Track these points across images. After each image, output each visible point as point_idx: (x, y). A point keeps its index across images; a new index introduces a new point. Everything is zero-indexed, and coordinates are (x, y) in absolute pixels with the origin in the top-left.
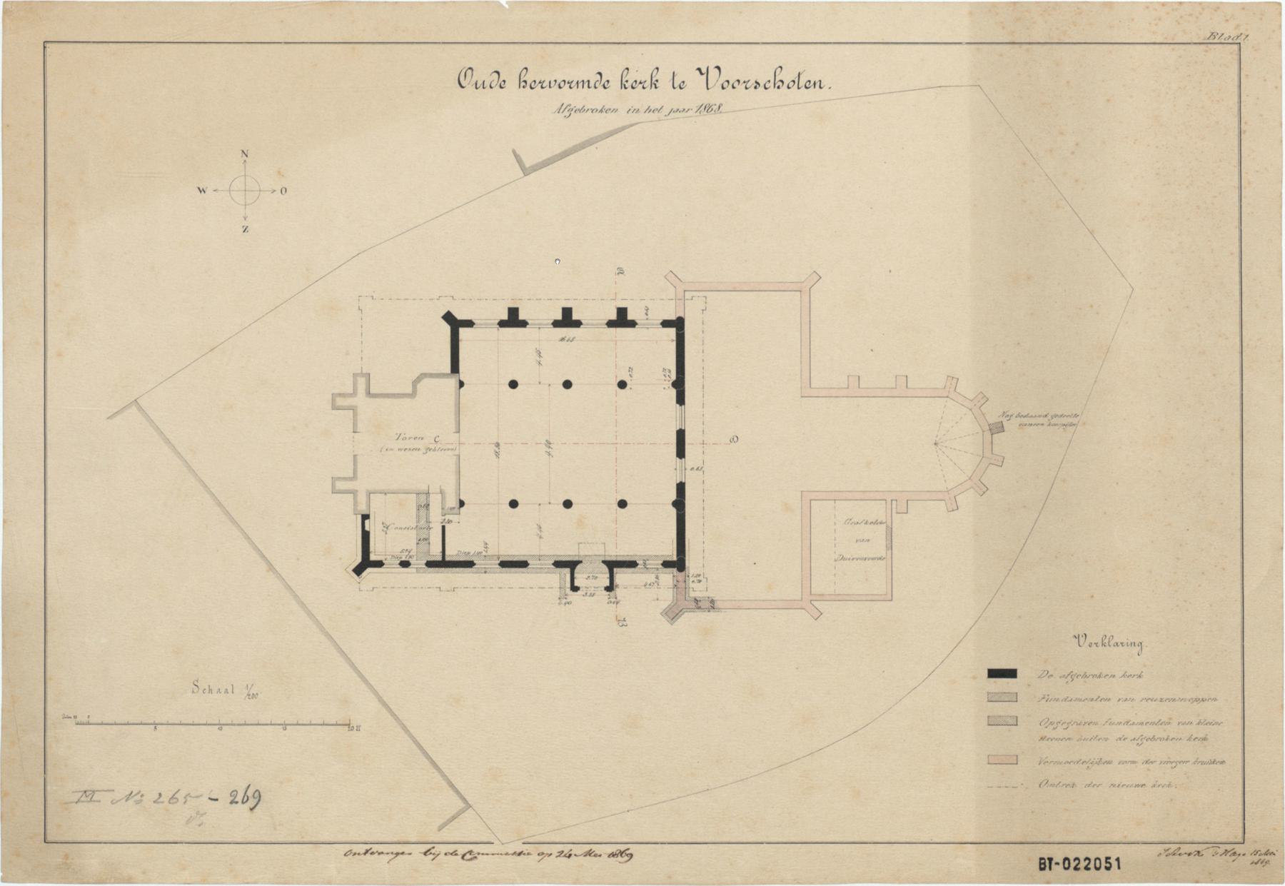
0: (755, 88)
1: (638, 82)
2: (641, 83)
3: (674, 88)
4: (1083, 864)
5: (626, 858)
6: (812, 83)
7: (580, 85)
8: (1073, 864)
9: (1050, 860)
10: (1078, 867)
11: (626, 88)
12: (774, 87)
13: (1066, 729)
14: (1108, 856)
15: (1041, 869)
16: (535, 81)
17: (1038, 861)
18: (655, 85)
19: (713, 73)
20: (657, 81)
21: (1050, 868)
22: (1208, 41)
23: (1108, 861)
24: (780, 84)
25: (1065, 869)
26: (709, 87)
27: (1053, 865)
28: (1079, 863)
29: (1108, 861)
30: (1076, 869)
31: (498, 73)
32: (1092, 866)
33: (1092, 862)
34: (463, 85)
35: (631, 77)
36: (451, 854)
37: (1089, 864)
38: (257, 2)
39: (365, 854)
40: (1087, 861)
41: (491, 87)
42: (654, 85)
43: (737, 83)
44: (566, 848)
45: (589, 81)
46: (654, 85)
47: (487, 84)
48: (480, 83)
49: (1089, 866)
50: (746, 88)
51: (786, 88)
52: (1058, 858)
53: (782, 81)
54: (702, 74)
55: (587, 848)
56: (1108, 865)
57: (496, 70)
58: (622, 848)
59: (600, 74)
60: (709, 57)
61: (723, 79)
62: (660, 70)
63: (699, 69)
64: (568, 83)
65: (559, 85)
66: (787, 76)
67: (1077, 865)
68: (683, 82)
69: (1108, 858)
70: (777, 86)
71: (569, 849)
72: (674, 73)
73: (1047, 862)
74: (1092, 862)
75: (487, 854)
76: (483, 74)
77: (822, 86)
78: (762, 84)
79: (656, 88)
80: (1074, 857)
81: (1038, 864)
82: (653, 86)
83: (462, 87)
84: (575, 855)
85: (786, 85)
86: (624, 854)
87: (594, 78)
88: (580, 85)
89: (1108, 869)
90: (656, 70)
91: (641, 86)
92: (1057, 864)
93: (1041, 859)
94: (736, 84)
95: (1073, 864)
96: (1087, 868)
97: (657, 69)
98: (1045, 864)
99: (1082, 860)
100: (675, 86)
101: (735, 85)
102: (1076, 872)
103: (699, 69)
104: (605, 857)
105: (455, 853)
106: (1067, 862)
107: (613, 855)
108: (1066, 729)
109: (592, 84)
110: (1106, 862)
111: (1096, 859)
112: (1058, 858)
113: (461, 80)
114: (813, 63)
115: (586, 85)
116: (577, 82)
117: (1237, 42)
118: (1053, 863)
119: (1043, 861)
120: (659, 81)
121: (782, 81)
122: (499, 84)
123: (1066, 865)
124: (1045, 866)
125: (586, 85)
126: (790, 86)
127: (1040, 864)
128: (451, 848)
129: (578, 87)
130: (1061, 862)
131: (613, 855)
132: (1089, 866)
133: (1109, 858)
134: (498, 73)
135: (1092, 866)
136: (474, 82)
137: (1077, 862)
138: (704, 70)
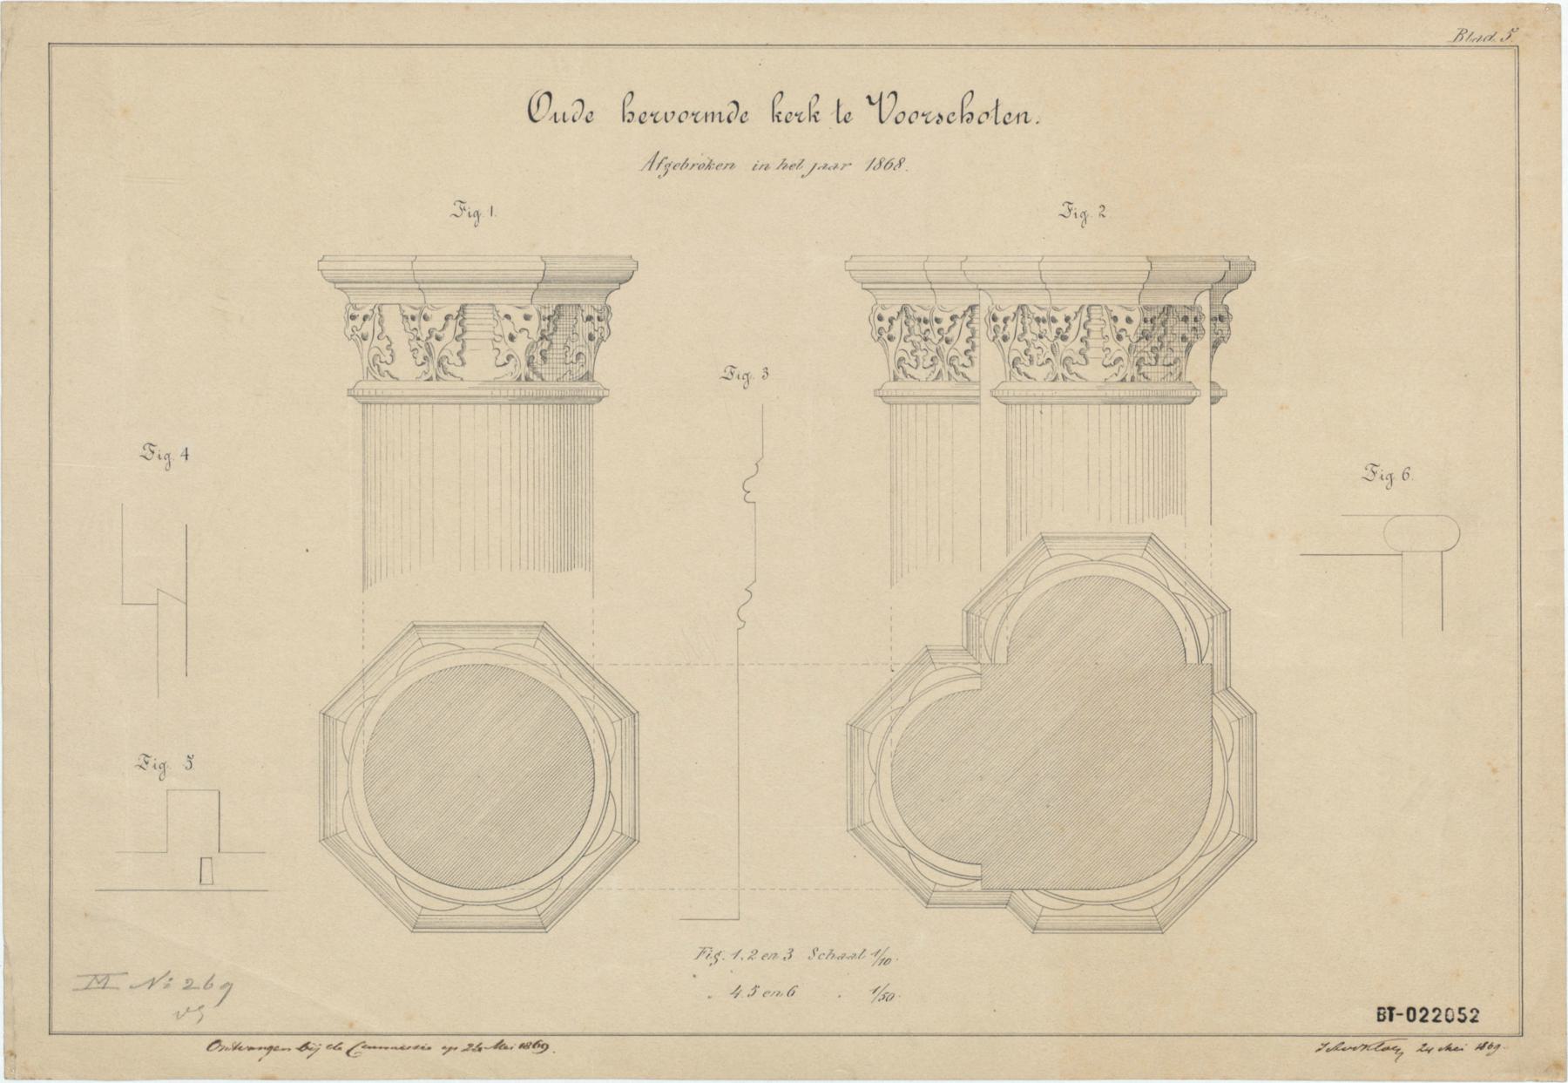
0: (937, 122)
2: (923, 115)
3: (838, 122)
4: (1431, 1016)
5: (540, 1049)
6: (1014, 116)
7: (709, 118)
8: (1419, 1015)
9: (1391, 1009)
10: (1426, 1019)
11: (779, 121)
12: (624, 120)
16: (645, 113)
17: (1377, 1011)
18: (815, 117)
19: (888, 103)
21: (1391, 1019)
24: (970, 116)
25: (1410, 1021)
26: (883, 120)
27: (1395, 1017)
31: (582, 101)
32: (1442, 1018)
34: (535, 118)
36: (334, 1048)
38: (895, 5)
39: (410, 1047)
40: (1424, 1012)
41: (574, 121)
42: (814, 117)
43: (985, 116)
44: (476, 1041)
45: (720, 113)
46: (814, 117)
48: (559, 117)
50: (927, 122)
51: (677, 121)
53: (632, 113)
54: (871, 103)
56: (1462, 1017)
57: (580, 98)
59: (736, 103)
61: (899, 109)
62: (784, 95)
63: (869, 97)
64: (796, 115)
65: (741, 118)
66: (976, 107)
68: (850, 113)
70: (626, 119)
73: (1388, 1012)
74: (1443, 1012)
75: (386, 1048)
76: (562, 104)
77: (1028, 120)
79: (816, 121)
83: (535, 121)
84: (486, 1048)
85: (637, 117)
88: (709, 118)
90: (780, 95)
93: (1379, 1008)
95: (1419, 1015)
97: (782, 93)
100: (840, 120)
101: (982, 120)
103: (869, 97)
105: (337, 1047)
106: (1411, 1012)
107: (522, 1046)
109: (724, 117)
110: (1460, 1013)
111: (1447, 1010)
115: (717, 119)
116: (1018, 116)
118: (1394, 1012)
119: (1382, 1011)
120: (820, 114)
121: (632, 113)
123: (1411, 1017)
124: (1385, 1017)
125: (717, 119)
126: (899, 120)
127: (1379, 1014)
128: (335, 1041)
129: (1018, 122)
130: (1405, 1012)
131: (522, 1046)
134: (582, 101)
135: (1442, 1018)
136: (553, 114)
137: (1424, 1012)
138: (875, 99)
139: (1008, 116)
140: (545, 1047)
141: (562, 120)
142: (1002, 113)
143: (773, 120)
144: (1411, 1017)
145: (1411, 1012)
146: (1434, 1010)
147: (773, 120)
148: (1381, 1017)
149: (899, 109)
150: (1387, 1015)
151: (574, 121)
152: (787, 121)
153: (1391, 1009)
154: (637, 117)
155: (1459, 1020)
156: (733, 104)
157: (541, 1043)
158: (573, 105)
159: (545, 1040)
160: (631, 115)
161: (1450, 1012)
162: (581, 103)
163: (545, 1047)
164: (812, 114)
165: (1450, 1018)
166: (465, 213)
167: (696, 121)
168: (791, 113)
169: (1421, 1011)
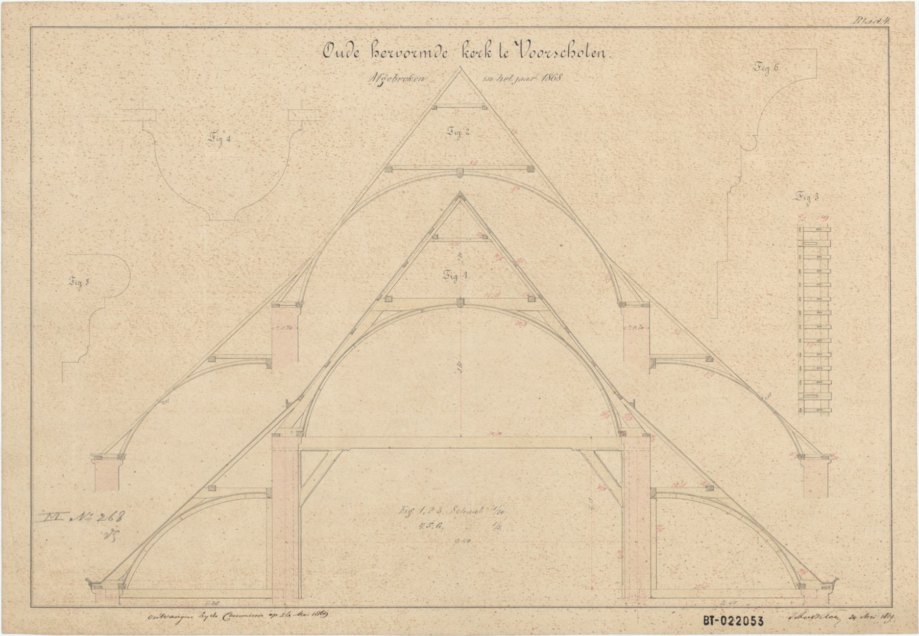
1: (475, 53)
3: (501, 57)
4: (736, 621)
6: (597, 52)
7: (423, 54)
9: (712, 617)
13: (114, 540)
14: (753, 615)
15: (706, 624)
19: (525, 45)
20: (490, 51)
21: (712, 624)
22: (854, 25)
23: (754, 619)
24: (377, 53)
26: (523, 56)
28: (732, 621)
29: (754, 619)
30: (731, 624)
33: (742, 619)
35: (470, 49)
37: (739, 621)
42: (488, 55)
45: (430, 51)
46: (488, 55)
47: (345, 54)
48: (339, 53)
49: (740, 623)
52: (718, 616)
54: (517, 45)
55: (300, 610)
56: (753, 622)
58: (321, 610)
60: (521, 35)
61: (532, 49)
67: (731, 622)
69: (753, 617)
71: (289, 611)
72: (588, 44)
73: (710, 618)
74: (742, 619)
78: (559, 54)
80: (729, 616)
81: (703, 620)
82: (465, 55)
86: (323, 614)
87: (436, 50)
89: (753, 625)
90: (467, 42)
91: (478, 55)
92: (717, 620)
93: (705, 617)
94: (581, 54)
95: (728, 621)
96: (738, 624)
98: (708, 620)
99: (735, 618)
100: (502, 56)
102: (738, 626)
103: (516, 42)
104: (310, 616)
106: (724, 619)
108: (114, 540)
110: (752, 620)
111: (744, 618)
112: (718, 616)
113: (325, 51)
114: (596, 40)
117: (885, 25)
118: (714, 619)
121: (377, 52)
122: (353, 53)
123: (724, 621)
125: (428, 55)
127: (705, 620)
130: (720, 619)
132: (740, 623)
133: (754, 617)
135: (742, 622)
137: (731, 619)
138: (519, 42)
139: (473, 53)
140: (326, 614)
141: (346, 56)
142: (590, 52)
143: (463, 57)
144: (724, 621)
145: (724, 619)
146: (729, 618)
147: (463, 57)
148: (706, 622)
149: (532, 49)
150: (710, 621)
151: (348, 57)
152: (505, 57)
153: (712, 617)
154: (577, 54)
155: (759, 624)
156: (439, 46)
157: (324, 612)
158: (436, 47)
159: (326, 610)
160: (573, 53)
161: (746, 619)
162: (440, 47)
163: (326, 614)
164: (464, 52)
165: (746, 622)
166: (595, 106)
167: (414, 56)
168: (385, 52)
169: (729, 618)
